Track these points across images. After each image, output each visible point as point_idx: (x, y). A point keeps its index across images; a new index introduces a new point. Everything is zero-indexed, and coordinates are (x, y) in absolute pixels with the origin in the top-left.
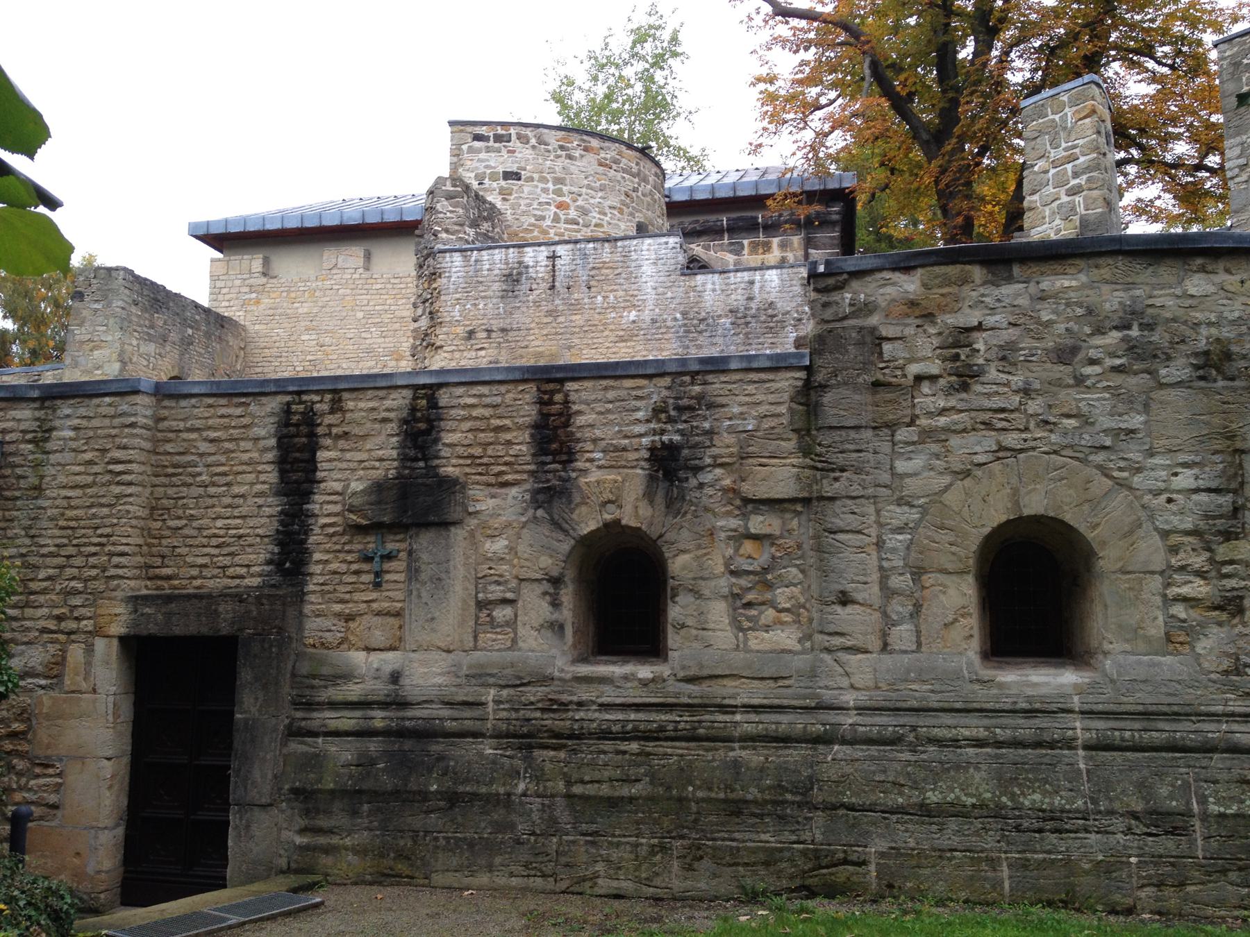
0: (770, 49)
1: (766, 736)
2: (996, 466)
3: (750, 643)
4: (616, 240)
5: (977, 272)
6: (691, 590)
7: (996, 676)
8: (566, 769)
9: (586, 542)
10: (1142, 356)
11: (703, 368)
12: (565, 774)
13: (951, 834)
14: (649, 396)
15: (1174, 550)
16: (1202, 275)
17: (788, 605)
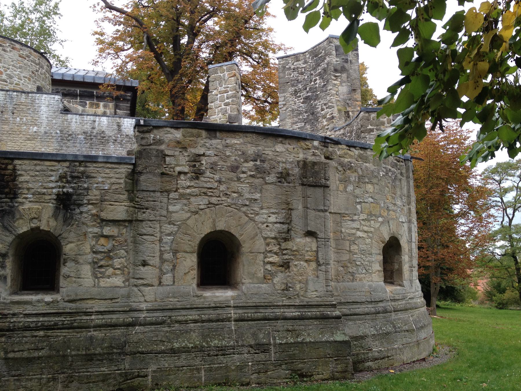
0: (103, 21)
1: (106, 325)
2: (207, 210)
3: (100, 284)
4: (28, 93)
5: (204, 133)
6: (74, 260)
7: (203, 294)
8: (5, 346)
9: (21, 237)
10: (260, 172)
11: (85, 159)
12: (4, 349)
13: (183, 360)
14: (58, 170)
15: (268, 244)
16: (281, 144)
17: (119, 267)
